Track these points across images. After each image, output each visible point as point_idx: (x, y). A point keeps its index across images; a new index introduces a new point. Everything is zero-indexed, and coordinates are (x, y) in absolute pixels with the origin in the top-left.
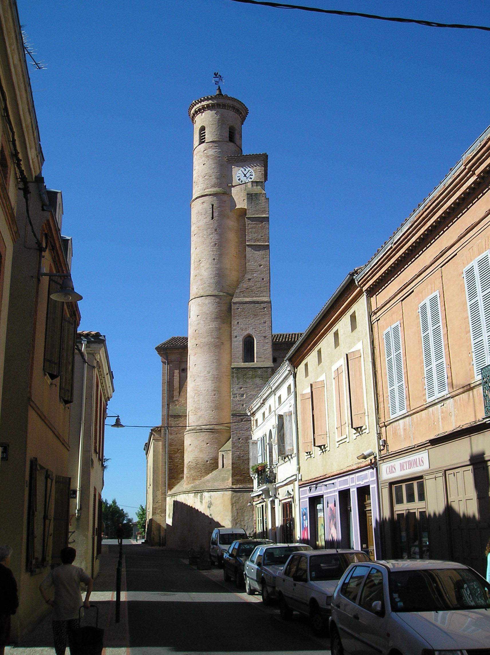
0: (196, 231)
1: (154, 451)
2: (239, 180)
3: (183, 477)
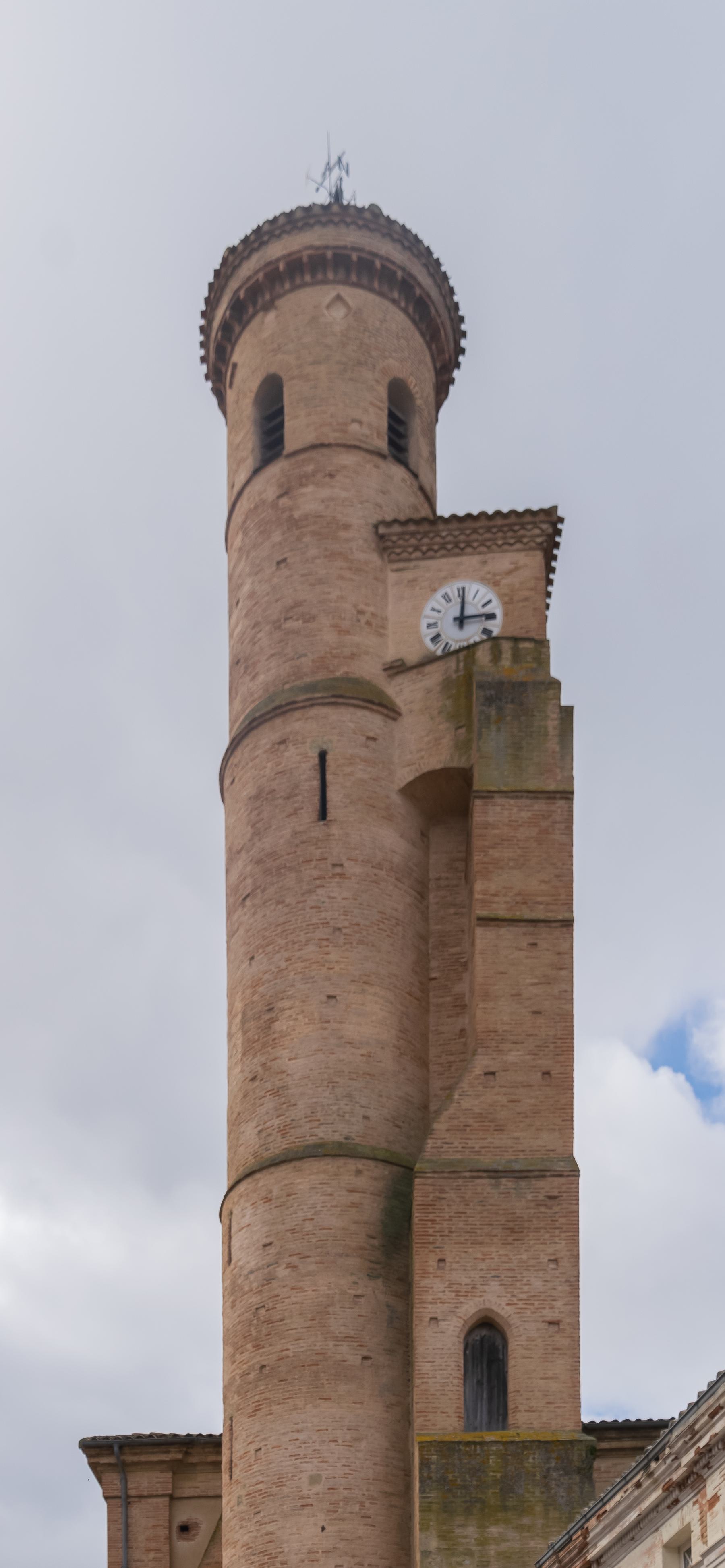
0: (249, 881)
2: (436, 639)
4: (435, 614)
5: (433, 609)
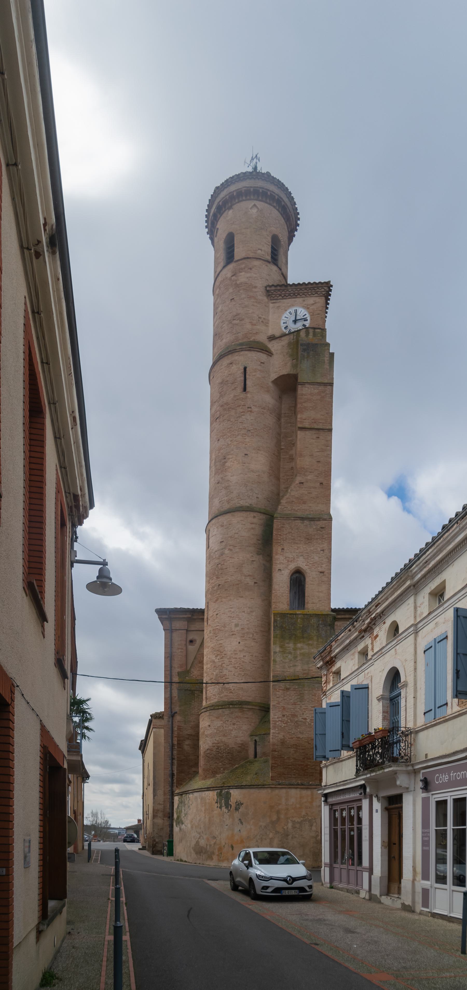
0: (218, 413)
1: (154, 742)
2: (286, 328)
3: (197, 773)
5: (285, 317)
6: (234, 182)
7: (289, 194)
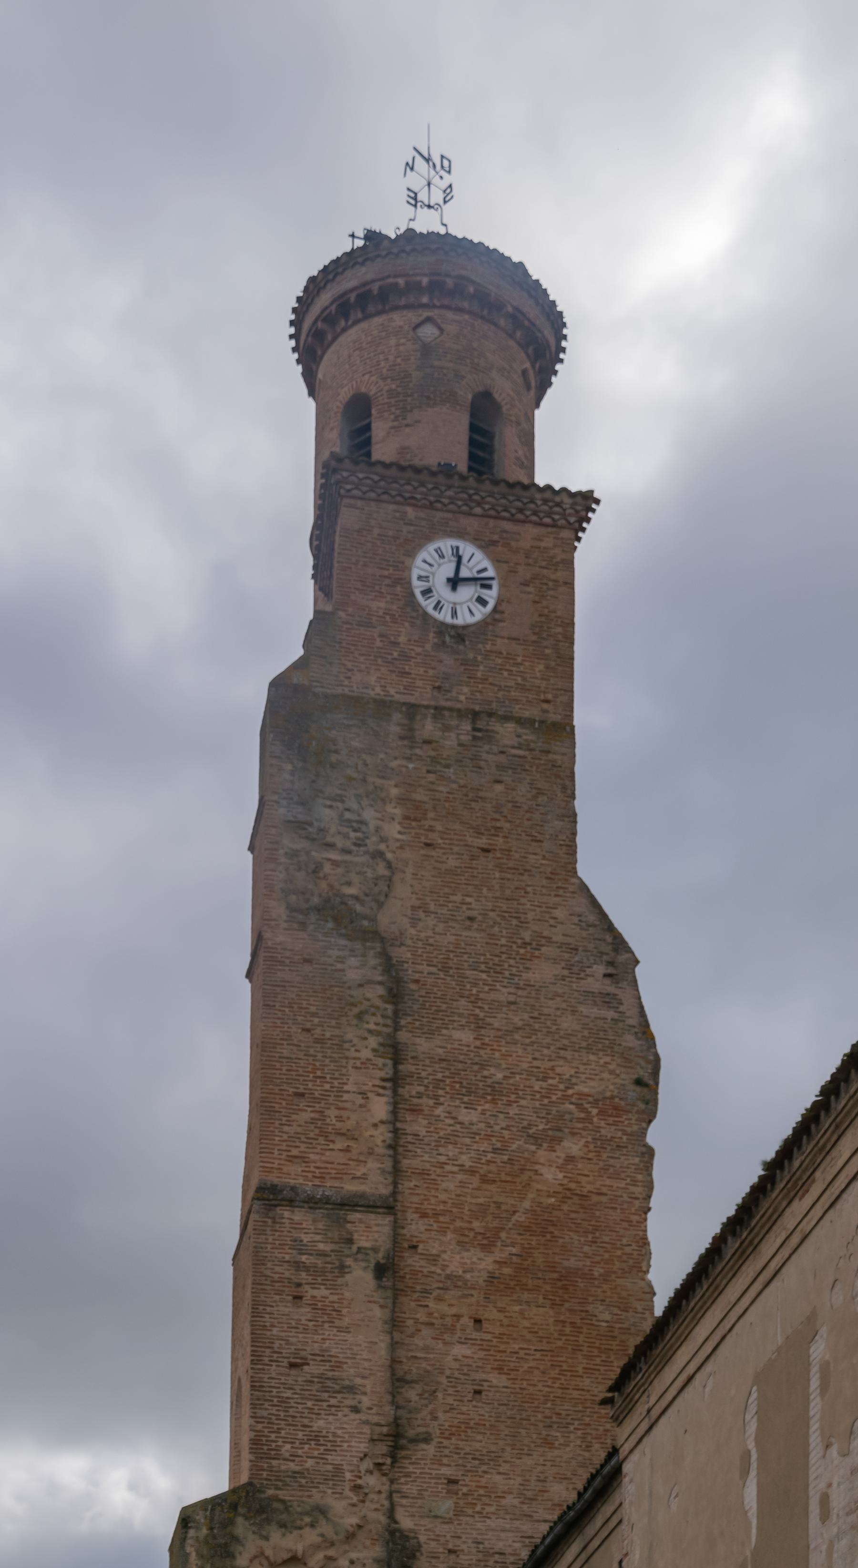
4: (426, 566)
5: (425, 561)
6: (340, 270)
7: (537, 291)
